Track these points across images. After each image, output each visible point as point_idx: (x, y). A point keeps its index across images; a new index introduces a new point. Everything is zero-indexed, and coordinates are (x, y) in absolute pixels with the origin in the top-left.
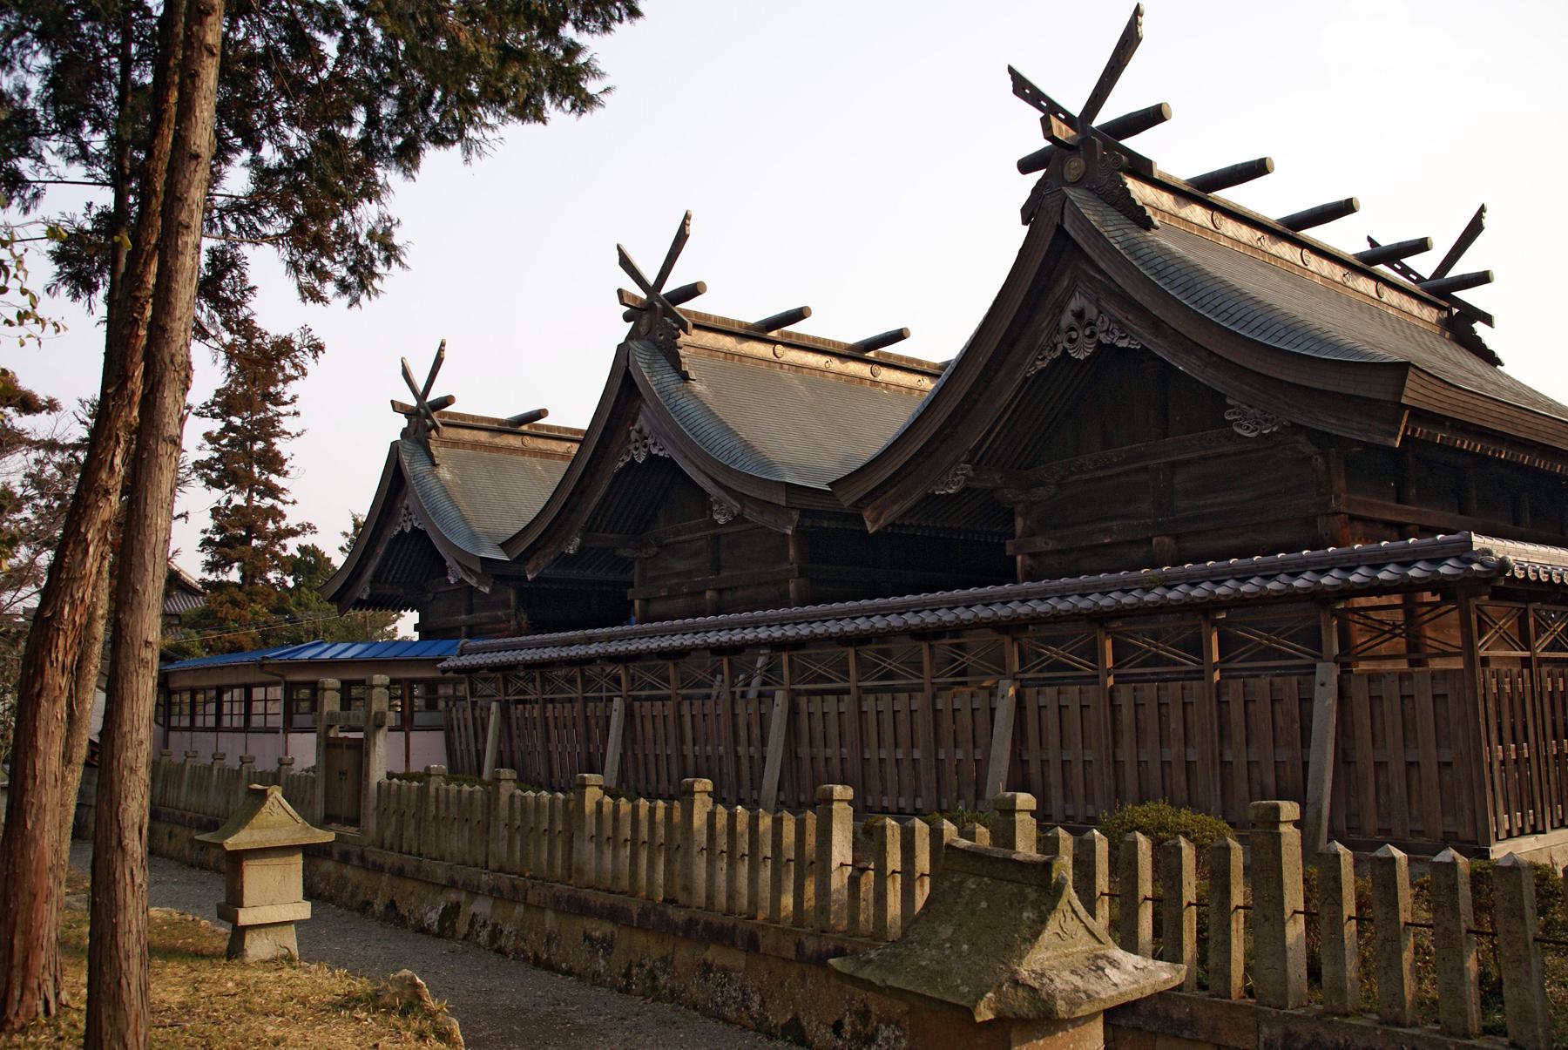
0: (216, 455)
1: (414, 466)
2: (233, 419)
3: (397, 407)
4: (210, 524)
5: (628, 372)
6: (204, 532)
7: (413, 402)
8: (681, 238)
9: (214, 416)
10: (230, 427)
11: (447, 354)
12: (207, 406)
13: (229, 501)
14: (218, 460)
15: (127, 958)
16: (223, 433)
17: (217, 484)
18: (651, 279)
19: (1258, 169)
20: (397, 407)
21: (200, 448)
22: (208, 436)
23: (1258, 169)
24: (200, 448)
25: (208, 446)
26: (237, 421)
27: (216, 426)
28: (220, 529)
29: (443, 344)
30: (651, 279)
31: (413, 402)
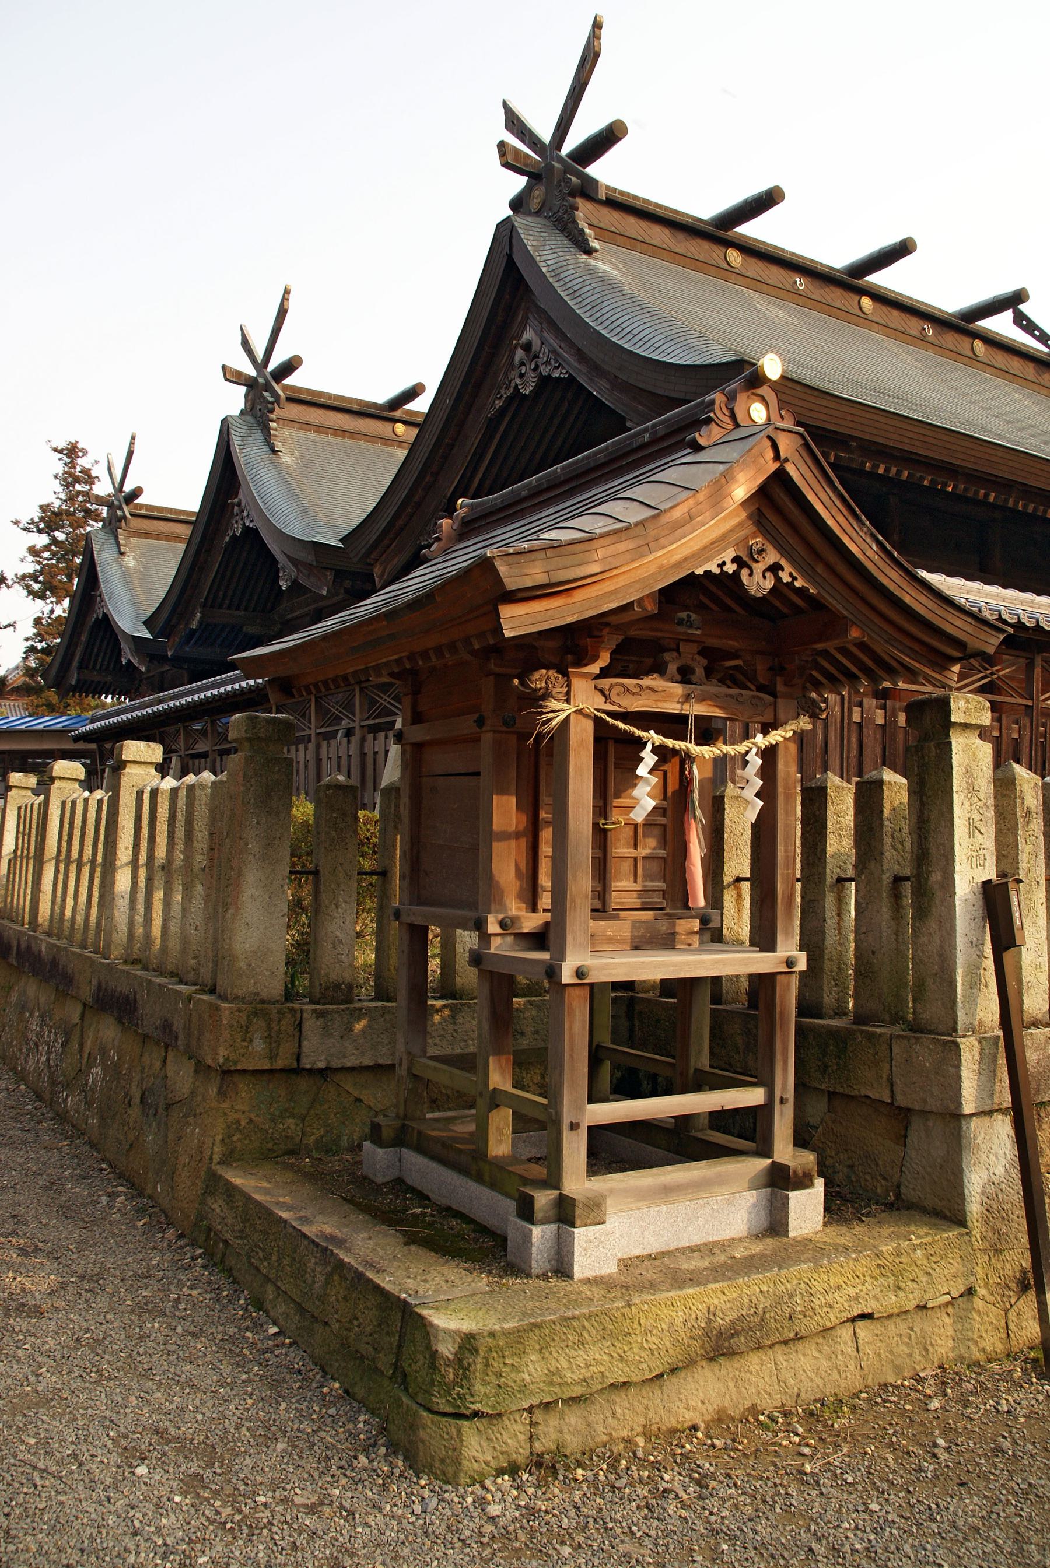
0: (38, 567)
1: (248, 453)
2: (57, 534)
3: (232, 376)
4: (31, 631)
5: (511, 265)
6: (27, 639)
7: (252, 372)
8: (589, 58)
9: (40, 531)
10: (55, 541)
11: (292, 305)
12: (32, 522)
13: (52, 611)
14: (42, 572)
15: (389, 949)
16: (47, 548)
17: (40, 595)
18: (546, 134)
19: (902, 250)
20: (232, 376)
21: (22, 560)
22: (33, 551)
23: (902, 250)
24: (22, 560)
25: (31, 558)
26: (60, 536)
27: (43, 540)
28: (40, 636)
29: (287, 292)
30: (546, 134)
31: (252, 372)
